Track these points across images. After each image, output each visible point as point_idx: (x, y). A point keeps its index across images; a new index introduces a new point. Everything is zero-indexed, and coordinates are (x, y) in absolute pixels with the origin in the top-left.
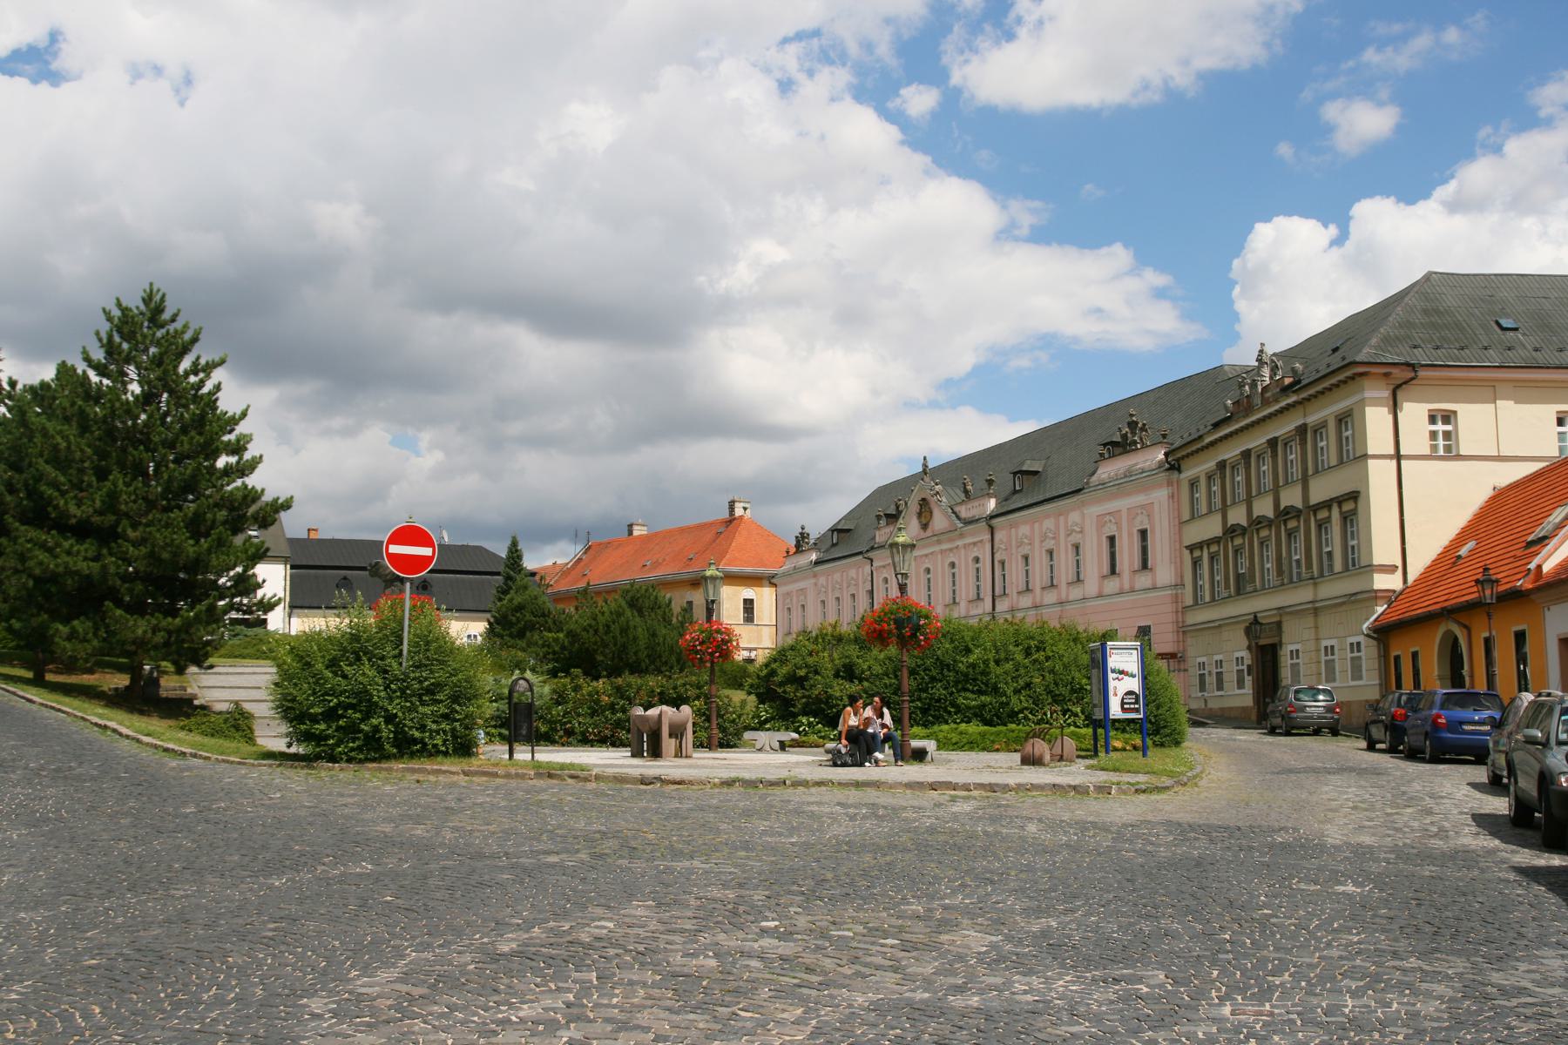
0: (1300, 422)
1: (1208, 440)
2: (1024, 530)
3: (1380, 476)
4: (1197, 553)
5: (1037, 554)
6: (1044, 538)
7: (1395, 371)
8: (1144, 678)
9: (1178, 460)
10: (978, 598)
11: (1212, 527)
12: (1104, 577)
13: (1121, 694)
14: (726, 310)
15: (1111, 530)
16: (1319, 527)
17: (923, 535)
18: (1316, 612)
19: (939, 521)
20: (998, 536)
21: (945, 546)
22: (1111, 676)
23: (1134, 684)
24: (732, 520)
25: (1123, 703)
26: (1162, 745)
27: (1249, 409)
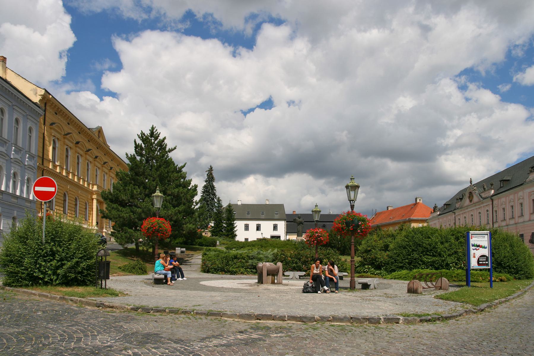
2: (503, 200)
5: (507, 208)
8: (491, 250)
10: (488, 223)
12: (531, 214)
13: (477, 256)
14: (444, 150)
17: (470, 204)
19: (475, 199)
20: (495, 202)
22: (472, 248)
23: (486, 252)
24: (416, 204)
25: (478, 261)
26: (519, 279)
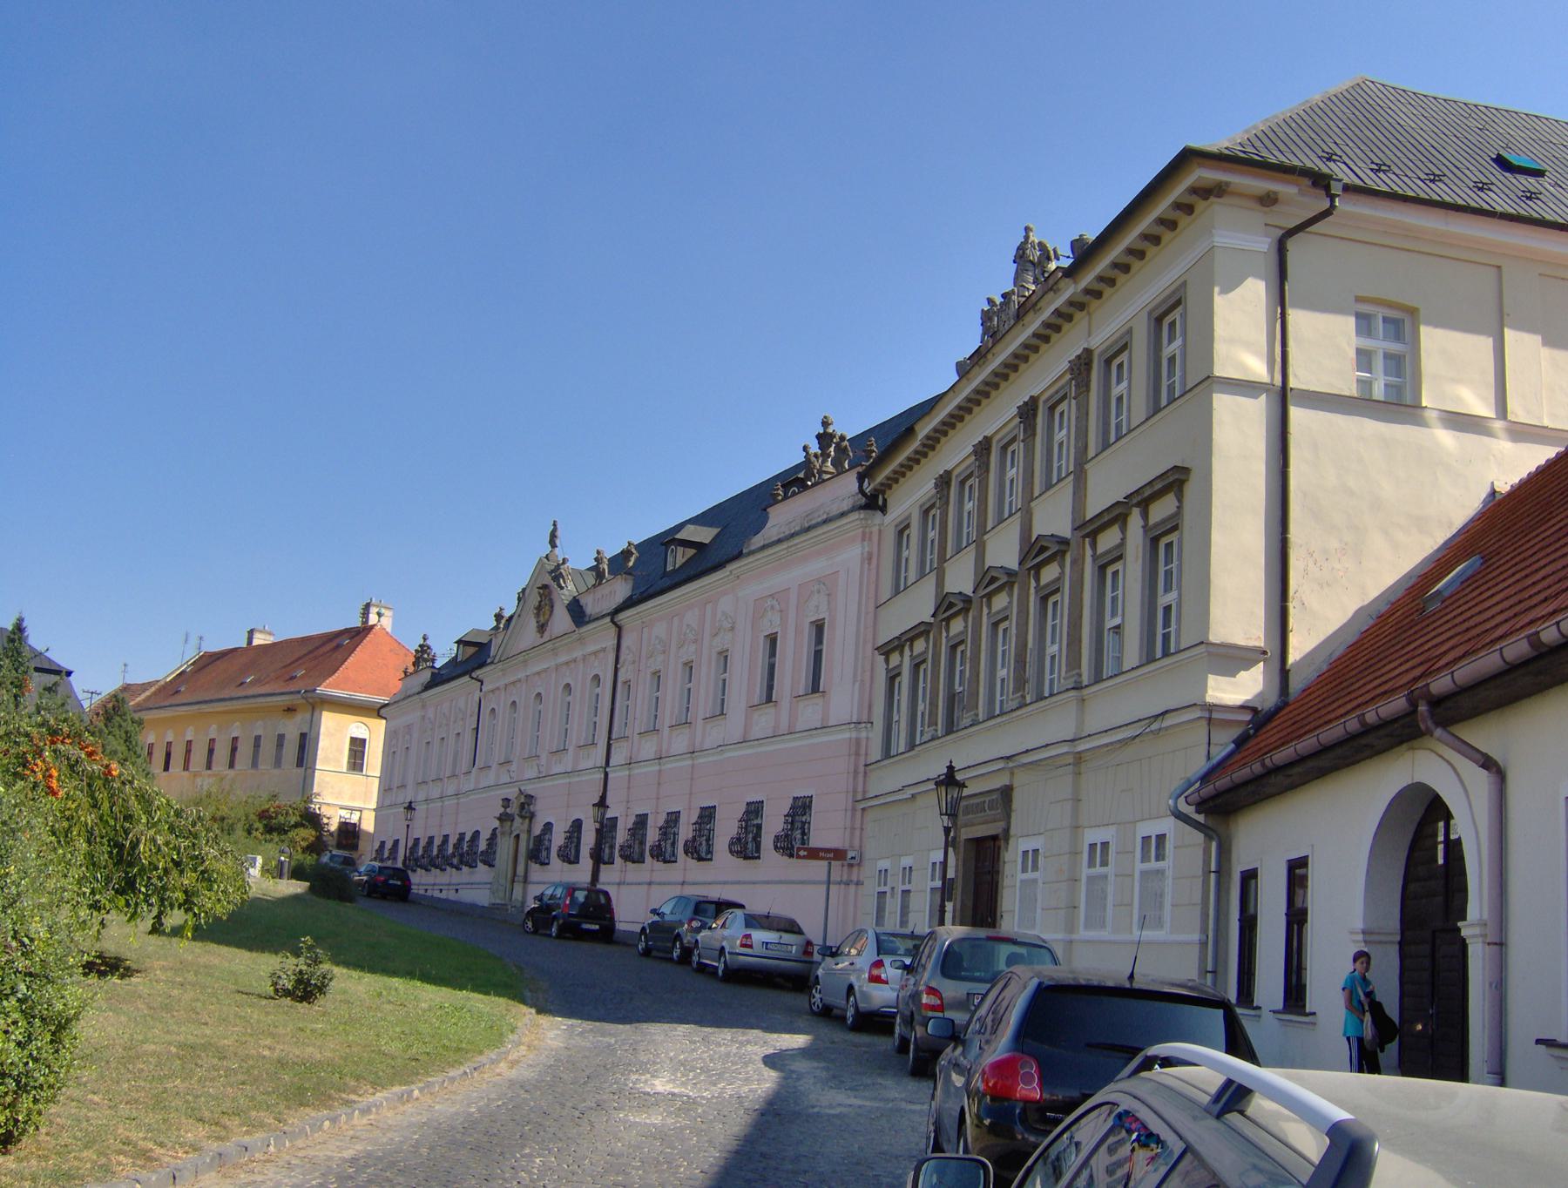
3: (1237, 429)
7: (1285, 189)
11: (919, 606)
15: (771, 624)
21: (563, 658)
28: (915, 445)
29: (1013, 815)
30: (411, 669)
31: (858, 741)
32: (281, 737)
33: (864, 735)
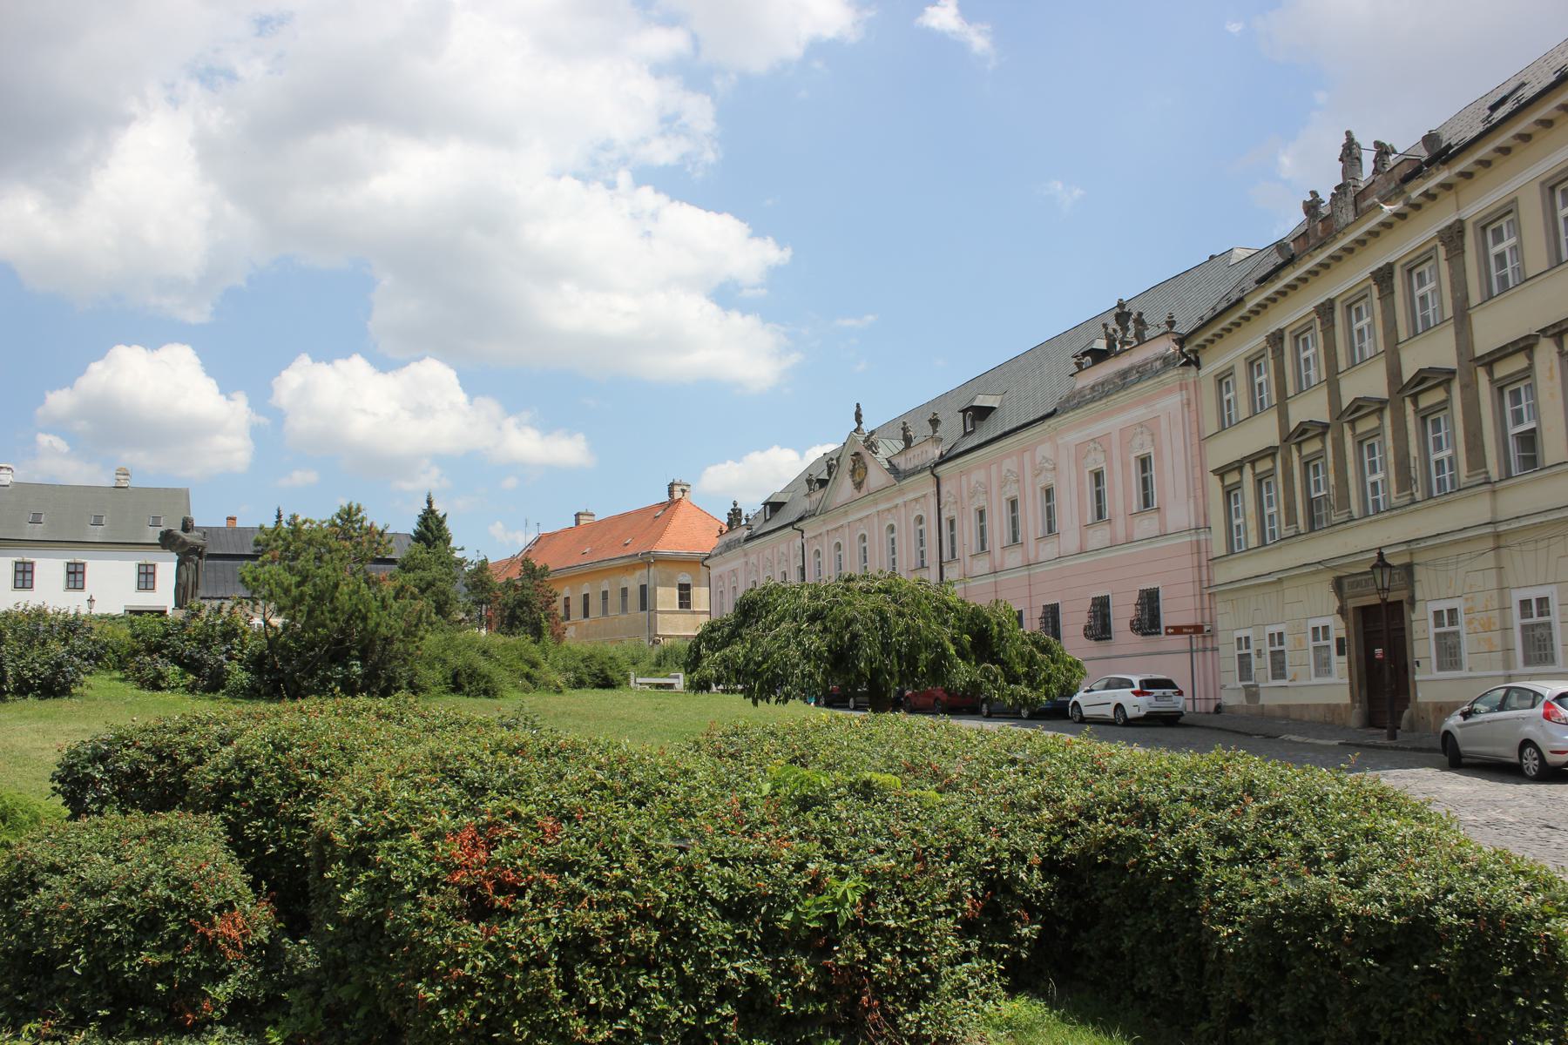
0: (1450, 220)
1: (1251, 304)
4: (1232, 478)
6: (1003, 483)
9: (1195, 352)
15: (1096, 461)
16: (1259, 483)
17: (857, 495)
18: (1499, 541)
27: (1331, 234)
28: (1243, 311)
29: (1417, 585)
30: (725, 529)
31: (1198, 542)
32: (624, 590)
33: (1203, 537)
